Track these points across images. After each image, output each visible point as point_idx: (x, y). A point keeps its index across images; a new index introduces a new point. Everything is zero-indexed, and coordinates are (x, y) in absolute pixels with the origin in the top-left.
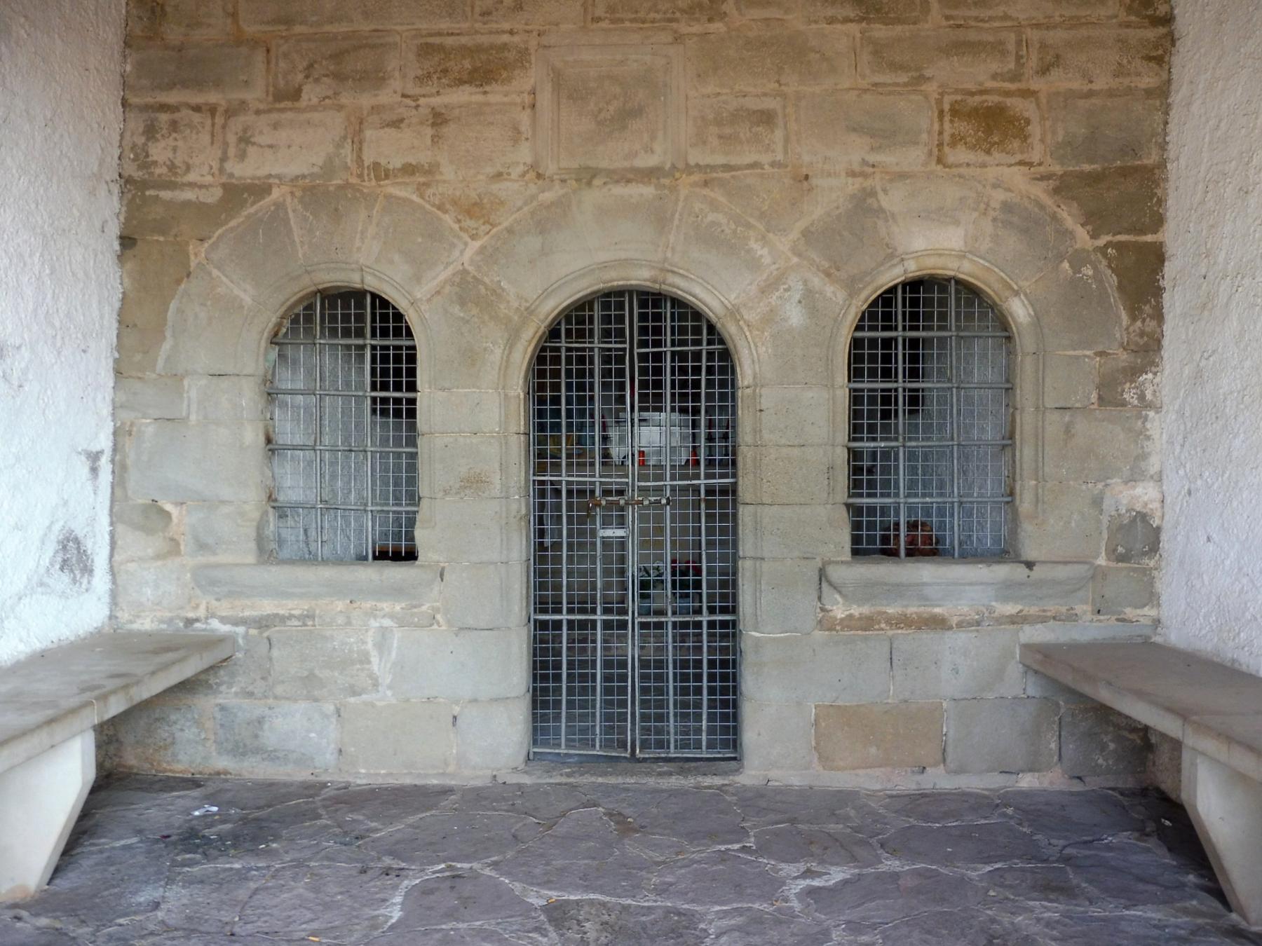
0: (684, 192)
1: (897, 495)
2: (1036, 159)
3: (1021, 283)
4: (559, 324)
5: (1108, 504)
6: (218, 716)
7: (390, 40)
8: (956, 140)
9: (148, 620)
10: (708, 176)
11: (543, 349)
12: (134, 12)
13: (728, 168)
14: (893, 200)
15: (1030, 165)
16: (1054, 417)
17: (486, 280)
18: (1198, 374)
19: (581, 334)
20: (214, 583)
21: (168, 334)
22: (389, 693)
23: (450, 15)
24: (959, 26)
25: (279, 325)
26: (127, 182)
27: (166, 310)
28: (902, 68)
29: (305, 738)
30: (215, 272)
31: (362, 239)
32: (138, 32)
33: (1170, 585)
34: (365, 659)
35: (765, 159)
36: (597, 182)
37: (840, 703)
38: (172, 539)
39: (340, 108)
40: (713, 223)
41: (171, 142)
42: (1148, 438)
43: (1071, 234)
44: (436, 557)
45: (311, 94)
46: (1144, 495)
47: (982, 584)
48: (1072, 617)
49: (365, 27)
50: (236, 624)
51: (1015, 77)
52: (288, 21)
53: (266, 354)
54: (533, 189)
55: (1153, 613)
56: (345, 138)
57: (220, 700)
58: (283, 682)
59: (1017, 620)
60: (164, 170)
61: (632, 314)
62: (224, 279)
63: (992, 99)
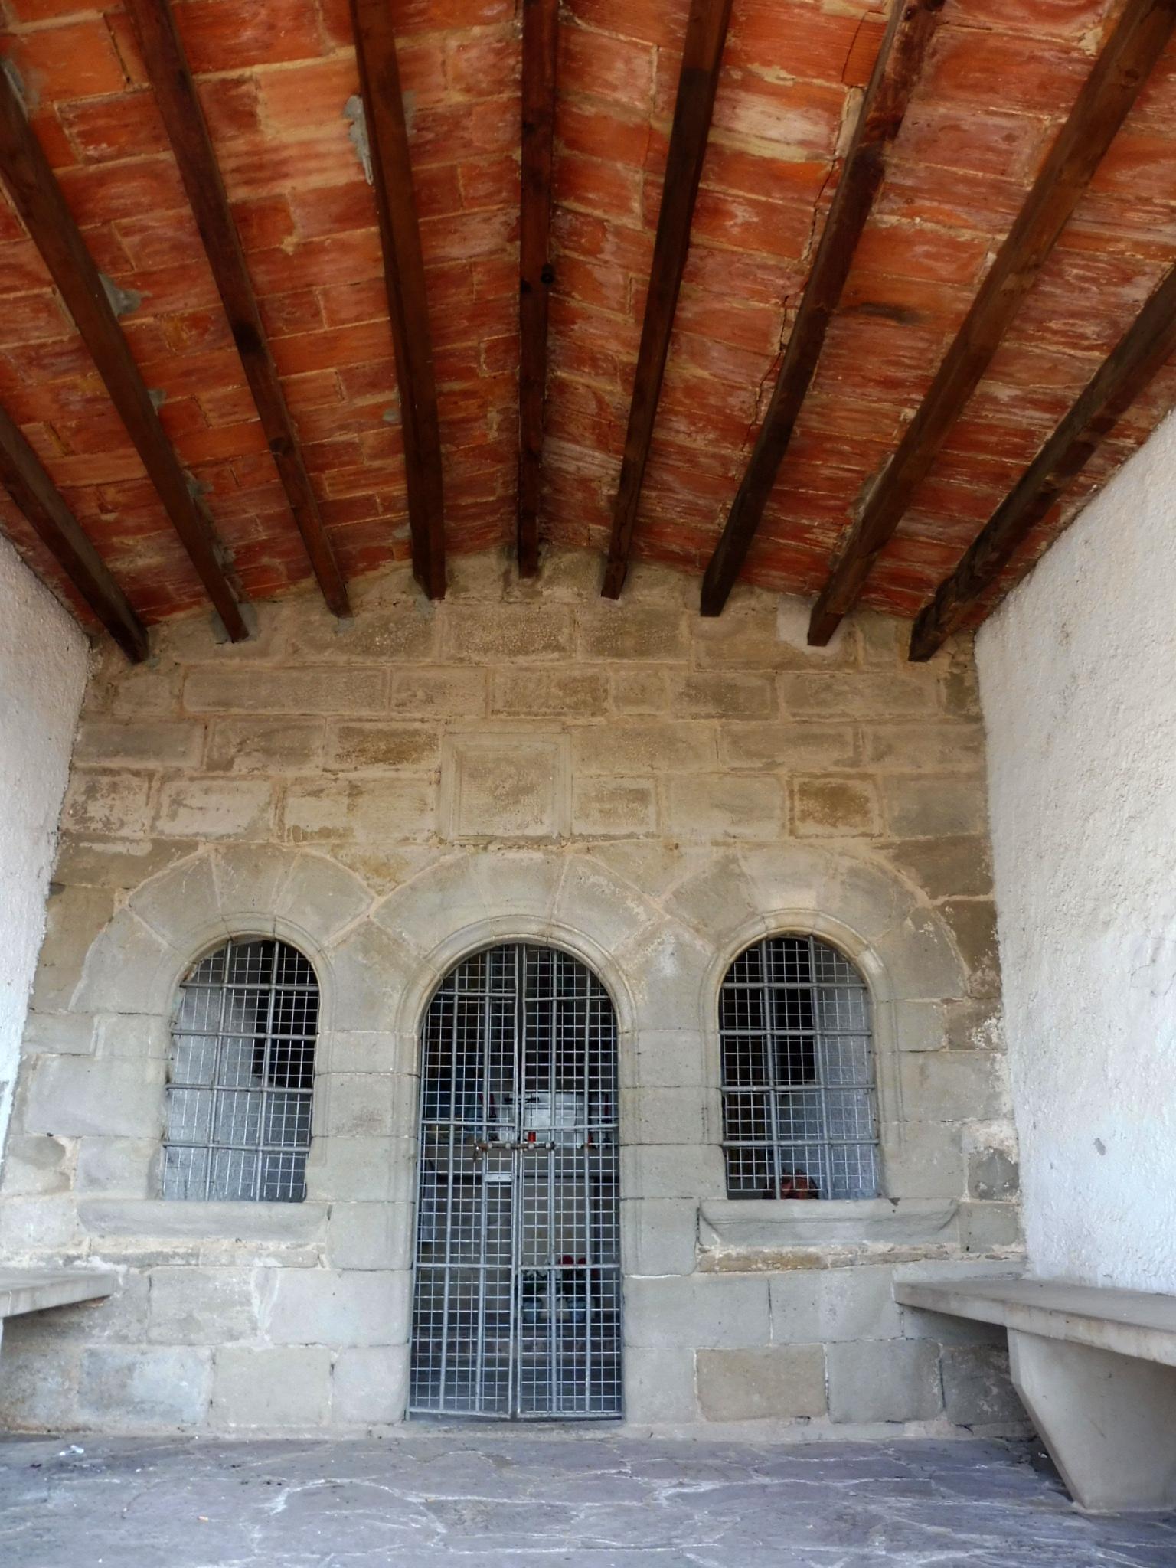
0: (568, 858)
1: (770, 1138)
2: (876, 832)
3: (870, 938)
4: (453, 974)
5: (966, 1141)
6: (86, 1363)
7: (317, 723)
8: (806, 815)
9: (27, 1257)
10: (590, 845)
11: (437, 998)
12: (92, 692)
13: (607, 837)
14: (753, 866)
15: (872, 836)
16: (910, 1059)
17: (389, 930)
18: (1029, 1017)
19: (473, 984)
20: (102, 1217)
21: (84, 973)
22: (267, 1338)
23: (370, 705)
24: (805, 722)
25: (190, 969)
26: (63, 833)
27: (86, 952)
28: (758, 755)
29: (175, 1382)
30: (137, 918)
31: (278, 893)
32: (92, 708)
33: (1031, 1219)
34: (246, 1301)
35: (640, 830)
36: (491, 847)
37: (721, 1347)
38: (62, 1174)
39: (267, 778)
40: (594, 885)
41: (109, 801)
42: (998, 1078)
43: (912, 896)
44: (324, 1195)
45: (241, 765)
46: (998, 1132)
47: (850, 1219)
48: (942, 1256)
49: (295, 711)
50: (117, 1262)
51: (855, 763)
52: (227, 704)
53: (175, 995)
54: (435, 852)
55: (1020, 1249)
56: (269, 804)
57: (90, 1345)
58: (160, 1325)
59: (888, 1259)
60: (100, 825)
61: (521, 967)
62: (144, 924)
63: (835, 782)
